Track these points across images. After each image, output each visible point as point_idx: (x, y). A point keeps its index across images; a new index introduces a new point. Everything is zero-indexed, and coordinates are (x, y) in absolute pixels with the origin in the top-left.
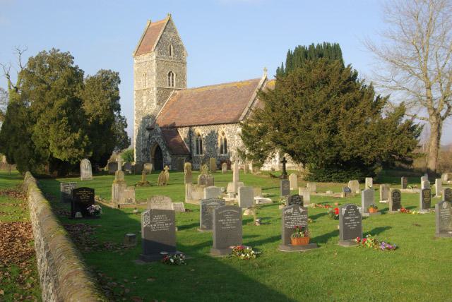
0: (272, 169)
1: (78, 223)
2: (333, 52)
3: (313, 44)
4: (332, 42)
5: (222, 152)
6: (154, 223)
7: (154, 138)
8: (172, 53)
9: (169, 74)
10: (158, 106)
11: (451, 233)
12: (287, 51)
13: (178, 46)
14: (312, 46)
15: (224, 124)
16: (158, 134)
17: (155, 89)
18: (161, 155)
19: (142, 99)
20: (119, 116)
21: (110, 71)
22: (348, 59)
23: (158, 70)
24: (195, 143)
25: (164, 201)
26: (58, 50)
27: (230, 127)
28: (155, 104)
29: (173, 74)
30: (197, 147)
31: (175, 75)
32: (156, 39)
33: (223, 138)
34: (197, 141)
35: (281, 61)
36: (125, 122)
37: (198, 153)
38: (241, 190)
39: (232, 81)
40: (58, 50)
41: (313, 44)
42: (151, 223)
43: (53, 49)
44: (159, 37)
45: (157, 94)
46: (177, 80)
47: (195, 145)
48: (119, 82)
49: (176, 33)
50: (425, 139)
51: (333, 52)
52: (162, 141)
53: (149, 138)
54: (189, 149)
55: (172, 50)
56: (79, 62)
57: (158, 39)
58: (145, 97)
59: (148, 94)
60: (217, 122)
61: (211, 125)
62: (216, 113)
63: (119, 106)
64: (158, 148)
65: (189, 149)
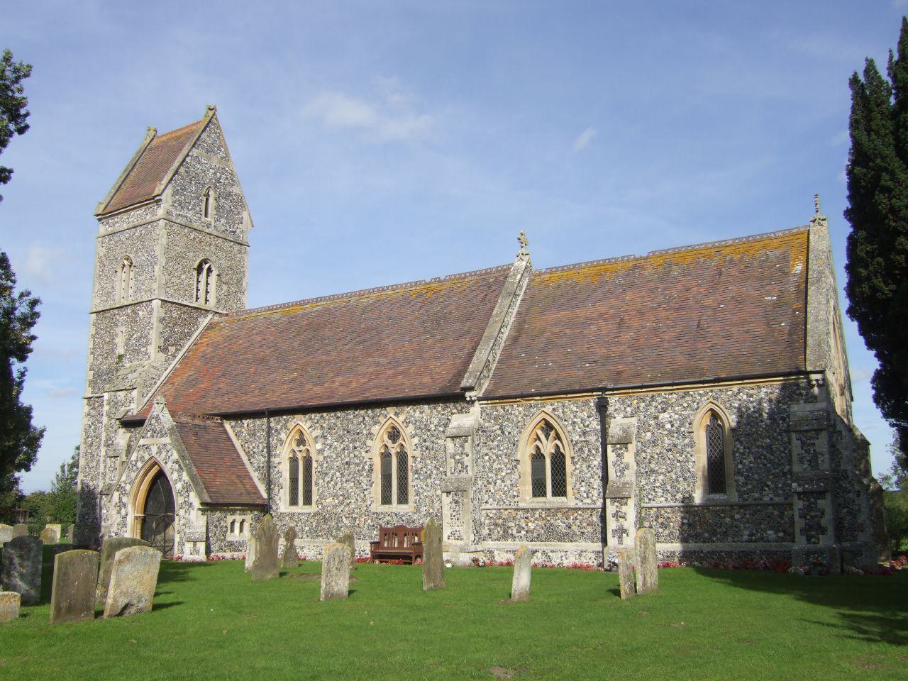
0: (613, 517)
1: (423, 539)
3: (870, 68)
7: (147, 447)
10: (162, 356)
13: (230, 194)
18: (170, 505)
24: (284, 469)
28: (152, 349)
29: (209, 270)
30: (294, 481)
31: (215, 272)
34: (294, 461)
37: (294, 501)
41: (870, 68)
44: (180, 159)
46: (219, 287)
49: (226, 158)
52: (175, 456)
53: (129, 450)
55: (211, 201)
57: (176, 164)
60: (372, 395)
62: (362, 370)
64: (161, 475)
65: (265, 496)
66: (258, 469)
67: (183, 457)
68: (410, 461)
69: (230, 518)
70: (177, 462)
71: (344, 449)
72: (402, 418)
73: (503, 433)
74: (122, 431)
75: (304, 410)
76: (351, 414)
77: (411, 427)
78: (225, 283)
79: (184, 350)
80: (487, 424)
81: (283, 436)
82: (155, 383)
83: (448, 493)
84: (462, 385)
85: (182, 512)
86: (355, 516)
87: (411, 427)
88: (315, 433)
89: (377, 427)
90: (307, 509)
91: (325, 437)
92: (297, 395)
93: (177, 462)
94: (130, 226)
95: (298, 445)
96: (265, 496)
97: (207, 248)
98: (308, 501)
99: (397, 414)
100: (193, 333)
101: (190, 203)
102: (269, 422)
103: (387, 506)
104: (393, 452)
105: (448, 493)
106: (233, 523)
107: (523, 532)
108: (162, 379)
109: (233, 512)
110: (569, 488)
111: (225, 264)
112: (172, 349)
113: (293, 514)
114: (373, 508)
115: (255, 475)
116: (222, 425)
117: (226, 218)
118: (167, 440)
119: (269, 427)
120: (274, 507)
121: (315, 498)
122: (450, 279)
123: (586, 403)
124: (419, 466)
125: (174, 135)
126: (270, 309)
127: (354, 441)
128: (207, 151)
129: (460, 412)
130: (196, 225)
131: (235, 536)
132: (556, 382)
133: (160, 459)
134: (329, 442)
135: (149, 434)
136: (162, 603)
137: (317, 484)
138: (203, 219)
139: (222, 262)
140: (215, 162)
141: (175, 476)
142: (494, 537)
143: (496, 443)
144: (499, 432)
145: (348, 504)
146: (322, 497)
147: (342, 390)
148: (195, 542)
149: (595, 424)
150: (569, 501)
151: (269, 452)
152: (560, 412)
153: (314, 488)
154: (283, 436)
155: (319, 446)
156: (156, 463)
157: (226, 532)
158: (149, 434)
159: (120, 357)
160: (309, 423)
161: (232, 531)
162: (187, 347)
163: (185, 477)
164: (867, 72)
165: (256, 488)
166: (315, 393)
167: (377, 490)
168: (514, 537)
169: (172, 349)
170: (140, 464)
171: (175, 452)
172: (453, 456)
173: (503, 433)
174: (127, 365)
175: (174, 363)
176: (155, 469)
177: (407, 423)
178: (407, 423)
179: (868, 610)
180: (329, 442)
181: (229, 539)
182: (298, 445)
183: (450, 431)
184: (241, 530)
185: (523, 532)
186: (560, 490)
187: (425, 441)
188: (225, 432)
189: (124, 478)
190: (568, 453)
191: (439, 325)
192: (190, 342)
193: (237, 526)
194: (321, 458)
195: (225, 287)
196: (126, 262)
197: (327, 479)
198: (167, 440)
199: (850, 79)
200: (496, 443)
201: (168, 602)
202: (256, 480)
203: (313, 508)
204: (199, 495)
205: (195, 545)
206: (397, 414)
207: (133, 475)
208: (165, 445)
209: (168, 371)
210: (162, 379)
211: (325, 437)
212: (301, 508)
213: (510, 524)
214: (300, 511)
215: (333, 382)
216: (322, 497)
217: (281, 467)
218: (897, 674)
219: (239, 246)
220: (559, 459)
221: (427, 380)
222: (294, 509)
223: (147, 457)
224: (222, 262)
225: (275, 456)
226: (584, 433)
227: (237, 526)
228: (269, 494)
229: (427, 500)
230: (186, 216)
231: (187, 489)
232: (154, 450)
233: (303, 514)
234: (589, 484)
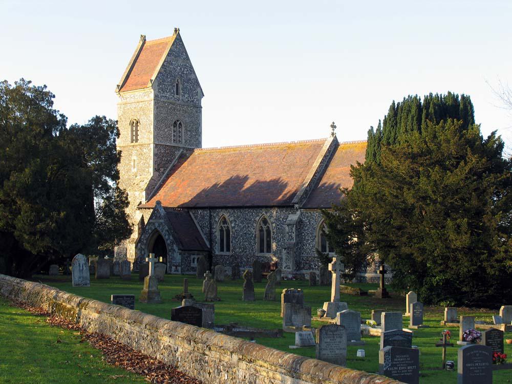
2: (456, 110)
4: (459, 91)
5: (262, 251)
6: (396, 365)
11: (243, 383)
12: (391, 104)
14: (429, 100)
16: (160, 218)
20: (118, 188)
21: (105, 118)
22: (488, 121)
24: (217, 234)
25: (338, 333)
26: (30, 82)
30: (222, 240)
32: (155, 67)
34: (222, 231)
36: (127, 198)
37: (222, 250)
40: (30, 82)
42: (393, 366)
43: (23, 80)
45: (155, 155)
47: (219, 237)
48: (118, 134)
50: (135, 170)
51: (456, 110)
52: (167, 228)
56: (60, 106)
60: (256, 203)
63: (118, 172)
65: (209, 247)
66: (205, 234)
67: (169, 229)
68: (272, 233)
69: (192, 257)
70: (167, 231)
71: (244, 227)
73: (310, 223)
75: (226, 208)
76: (247, 211)
78: (189, 131)
79: (168, 170)
80: (304, 219)
81: (217, 219)
82: (154, 188)
83: (285, 249)
84: (292, 202)
85: (170, 253)
86: (248, 257)
88: (232, 219)
89: (258, 218)
90: (228, 253)
91: (235, 221)
94: (136, 101)
95: (224, 224)
96: (209, 247)
97: (178, 113)
98: (228, 250)
99: (266, 213)
100: (172, 160)
101: (167, 88)
103: (262, 253)
104: (265, 229)
105: (285, 249)
106: (194, 259)
107: (317, 267)
108: (157, 185)
112: (162, 169)
113: (222, 255)
115: (204, 237)
116: (188, 212)
117: (189, 94)
118: (162, 221)
120: (213, 252)
121: (231, 248)
124: (276, 236)
127: (248, 224)
128: (176, 57)
129: (292, 213)
134: (237, 223)
135: (154, 218)
136: (175, 174)
137: (232, 242)
138: (176, 96)
139: (187, 119)
140: (180, 62)
141: (167, 237)
142: (305, 268)
143: (307, 228)
144: (308, 223)
145: (246, 252)
146: (234, 248)
148: (176, 266)
151: (211, 226)
153: (231, 244)
154: (217, 219)
155: (233, 225)
156: (158, 231)
157: (191, 262)
158: (154, 218)
160: (228, 214)
161: (194, 262)
162: (170, 168)
164: (430, 95)
165: (205, 243)
167: (257, 246)
169: (162, 169)
170: (150, 231)
171: (166, 227)
172: (288, 233)
173: (310, 223)
175: (163, 176)
179: (372, 292)
180: (237, 223)
181: (192, 266)
182: (224, 224)
183: (288, 222)
185: (317, 267)
187: (278, 225)
188: (190, 215)
189: (142, 237)
191: (290, 168)
192: (171, 165)
193: (196, 260)
194: (234, 230)
195: (189, 133)
197: (237, 240)
199: (370, 132)
200: (307, 228)
201: (169, 180)
202: (205, 239)
203: (230, 253)
205: (176, 268)
206: (266, 213)
208: (162, 223)
209: (160, 181)
210: (157, 185)
211: (235, 221)
212: (225, 253)
213: (312, 263)
214: (225, 254)
216: (234, 248)
217: (216, 234)
219: (196, 109)
222: (222, 253)
223: (153, 228)
224: (187, 119)
225: (213, 228)
227: (196, 260)
228: (211, 246)
229: (279, 252)
230: (166, 96)
231: (172, 243)
232: (157, 225)
233: (226, 256)
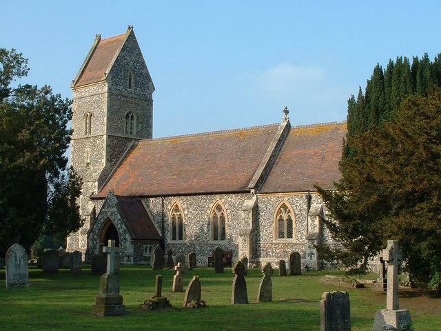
3: (426, 56)
8: (133, 85)
9: (127, 115)
15: (221, 193)
17: (105, 137)
19: (84, 152)
23: (109, 108)
27: (232, 199)
28: (104, 160)
31: (135, 118)
33: (285, 218)
35: (357, 83)
37: (174, 238)
38: (105, 271)
39: (253, 125)
45: (108, 146)
46: (137, 125)
52: (119, 217)
54: (160, 232)
55: (133, 80)
58: (87, 149)
59: (94, 146)
61: (200, 194)
65: (160, 232)
69: (145, 246)
70: (120, 220)
72: (223, 200)
74: (90, 202)
77: (227, 206)
85: (122, 243)
87: (227, 206)
92: (175, 187)
93: (120, 220)
102: (163, 200)
109: (146, 244)
110: (294, 235)
111: (140, 112)
112: (114, 160)
114: (210, 242)
115: (156, 225)
119: (163, 203)
122: (252, 129)
123: (302, 197)
125: (111, 40)
126: (164, 139)
129: (248, 199)
130: (124, 93)
131: (147, 254)
132: (290, 186)
133: (111, 218)
138: (128, 89)
147: (196, 184)
148: (129, 257)
149: (305, 207)
150: (293, 240)
152: (291, 201)
159: (88, 164)
163: (124, 227)
166: (184, 186)
168: (270, 256)
169: (114, 160)
172: (244, 219)
174: (92, 168)
176: (109, 224)
177: (225, 203)
178: (225, 203)
183: (244, 208)
184: (150, 252)
186: (290, 236)
190: (293, 218)
195: (140, 125)
196: (89, 114)
198: (115, 209)
204: (131, 235)
206: (220, 199)
207: (99, 225)
215: (193, 182)
218: (83, 183)
220: (290, 222)
221: (235, 183)
222: (174, 242)
226: (301, 210)
234: (302, 233)
